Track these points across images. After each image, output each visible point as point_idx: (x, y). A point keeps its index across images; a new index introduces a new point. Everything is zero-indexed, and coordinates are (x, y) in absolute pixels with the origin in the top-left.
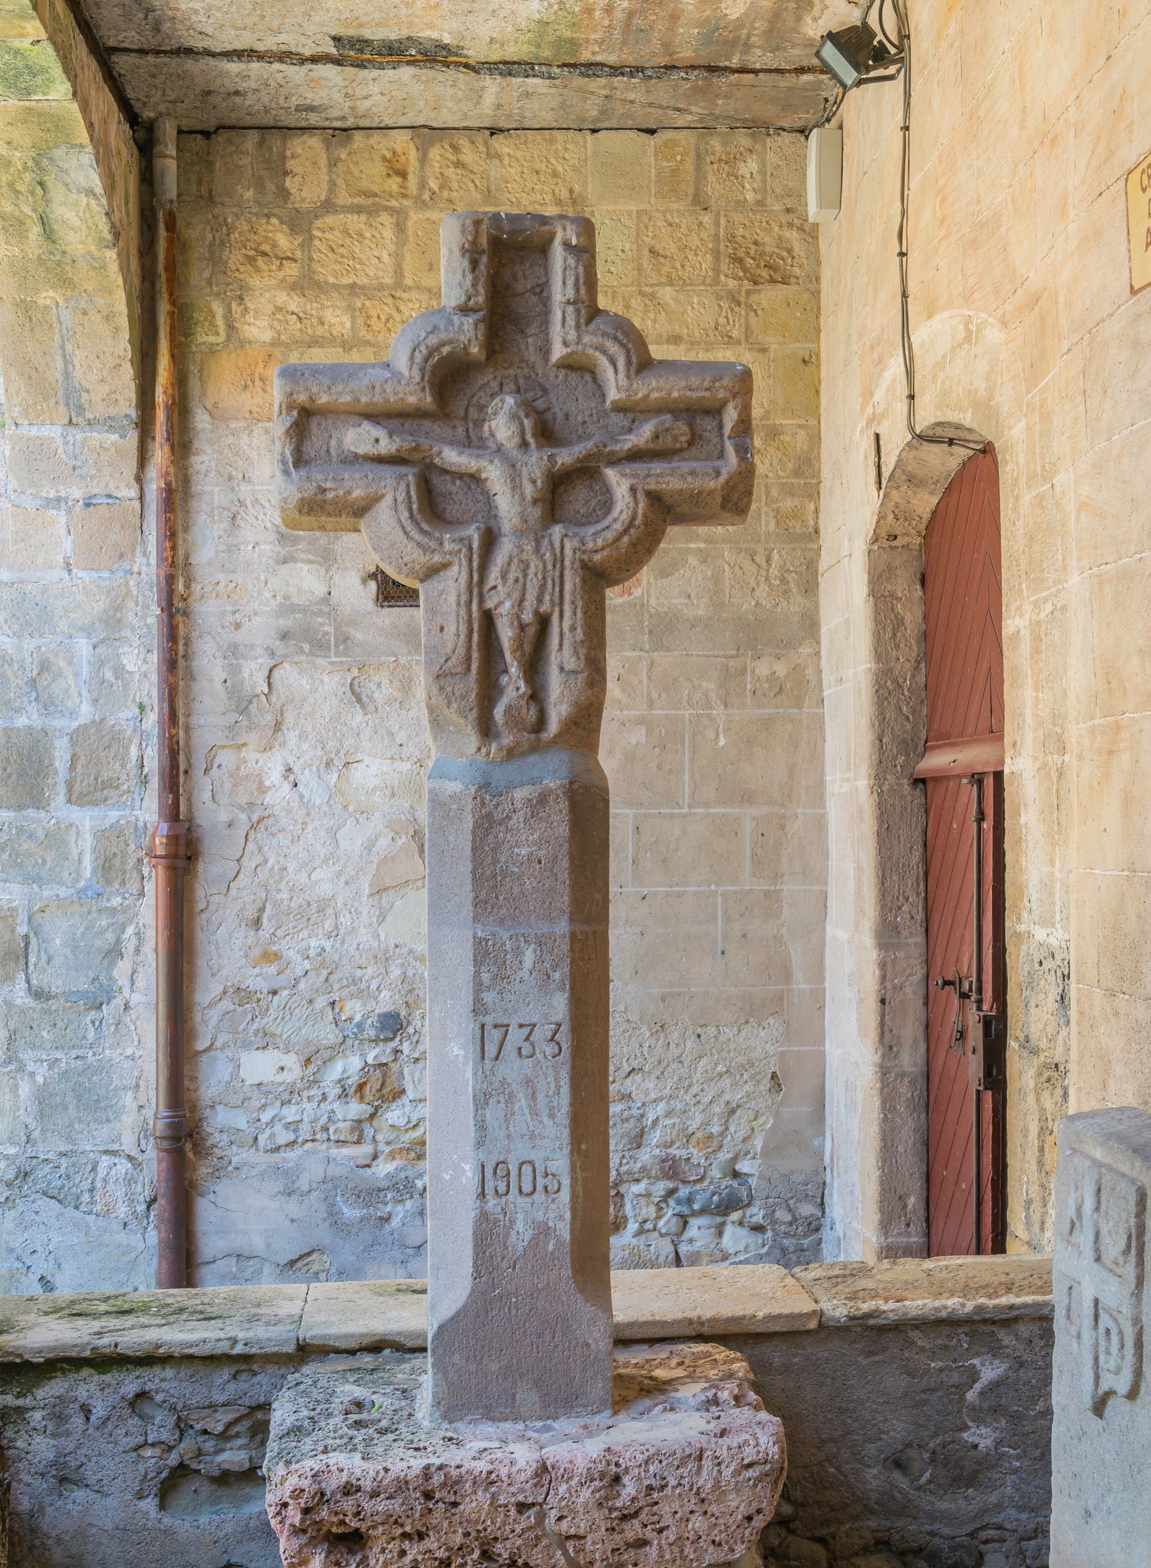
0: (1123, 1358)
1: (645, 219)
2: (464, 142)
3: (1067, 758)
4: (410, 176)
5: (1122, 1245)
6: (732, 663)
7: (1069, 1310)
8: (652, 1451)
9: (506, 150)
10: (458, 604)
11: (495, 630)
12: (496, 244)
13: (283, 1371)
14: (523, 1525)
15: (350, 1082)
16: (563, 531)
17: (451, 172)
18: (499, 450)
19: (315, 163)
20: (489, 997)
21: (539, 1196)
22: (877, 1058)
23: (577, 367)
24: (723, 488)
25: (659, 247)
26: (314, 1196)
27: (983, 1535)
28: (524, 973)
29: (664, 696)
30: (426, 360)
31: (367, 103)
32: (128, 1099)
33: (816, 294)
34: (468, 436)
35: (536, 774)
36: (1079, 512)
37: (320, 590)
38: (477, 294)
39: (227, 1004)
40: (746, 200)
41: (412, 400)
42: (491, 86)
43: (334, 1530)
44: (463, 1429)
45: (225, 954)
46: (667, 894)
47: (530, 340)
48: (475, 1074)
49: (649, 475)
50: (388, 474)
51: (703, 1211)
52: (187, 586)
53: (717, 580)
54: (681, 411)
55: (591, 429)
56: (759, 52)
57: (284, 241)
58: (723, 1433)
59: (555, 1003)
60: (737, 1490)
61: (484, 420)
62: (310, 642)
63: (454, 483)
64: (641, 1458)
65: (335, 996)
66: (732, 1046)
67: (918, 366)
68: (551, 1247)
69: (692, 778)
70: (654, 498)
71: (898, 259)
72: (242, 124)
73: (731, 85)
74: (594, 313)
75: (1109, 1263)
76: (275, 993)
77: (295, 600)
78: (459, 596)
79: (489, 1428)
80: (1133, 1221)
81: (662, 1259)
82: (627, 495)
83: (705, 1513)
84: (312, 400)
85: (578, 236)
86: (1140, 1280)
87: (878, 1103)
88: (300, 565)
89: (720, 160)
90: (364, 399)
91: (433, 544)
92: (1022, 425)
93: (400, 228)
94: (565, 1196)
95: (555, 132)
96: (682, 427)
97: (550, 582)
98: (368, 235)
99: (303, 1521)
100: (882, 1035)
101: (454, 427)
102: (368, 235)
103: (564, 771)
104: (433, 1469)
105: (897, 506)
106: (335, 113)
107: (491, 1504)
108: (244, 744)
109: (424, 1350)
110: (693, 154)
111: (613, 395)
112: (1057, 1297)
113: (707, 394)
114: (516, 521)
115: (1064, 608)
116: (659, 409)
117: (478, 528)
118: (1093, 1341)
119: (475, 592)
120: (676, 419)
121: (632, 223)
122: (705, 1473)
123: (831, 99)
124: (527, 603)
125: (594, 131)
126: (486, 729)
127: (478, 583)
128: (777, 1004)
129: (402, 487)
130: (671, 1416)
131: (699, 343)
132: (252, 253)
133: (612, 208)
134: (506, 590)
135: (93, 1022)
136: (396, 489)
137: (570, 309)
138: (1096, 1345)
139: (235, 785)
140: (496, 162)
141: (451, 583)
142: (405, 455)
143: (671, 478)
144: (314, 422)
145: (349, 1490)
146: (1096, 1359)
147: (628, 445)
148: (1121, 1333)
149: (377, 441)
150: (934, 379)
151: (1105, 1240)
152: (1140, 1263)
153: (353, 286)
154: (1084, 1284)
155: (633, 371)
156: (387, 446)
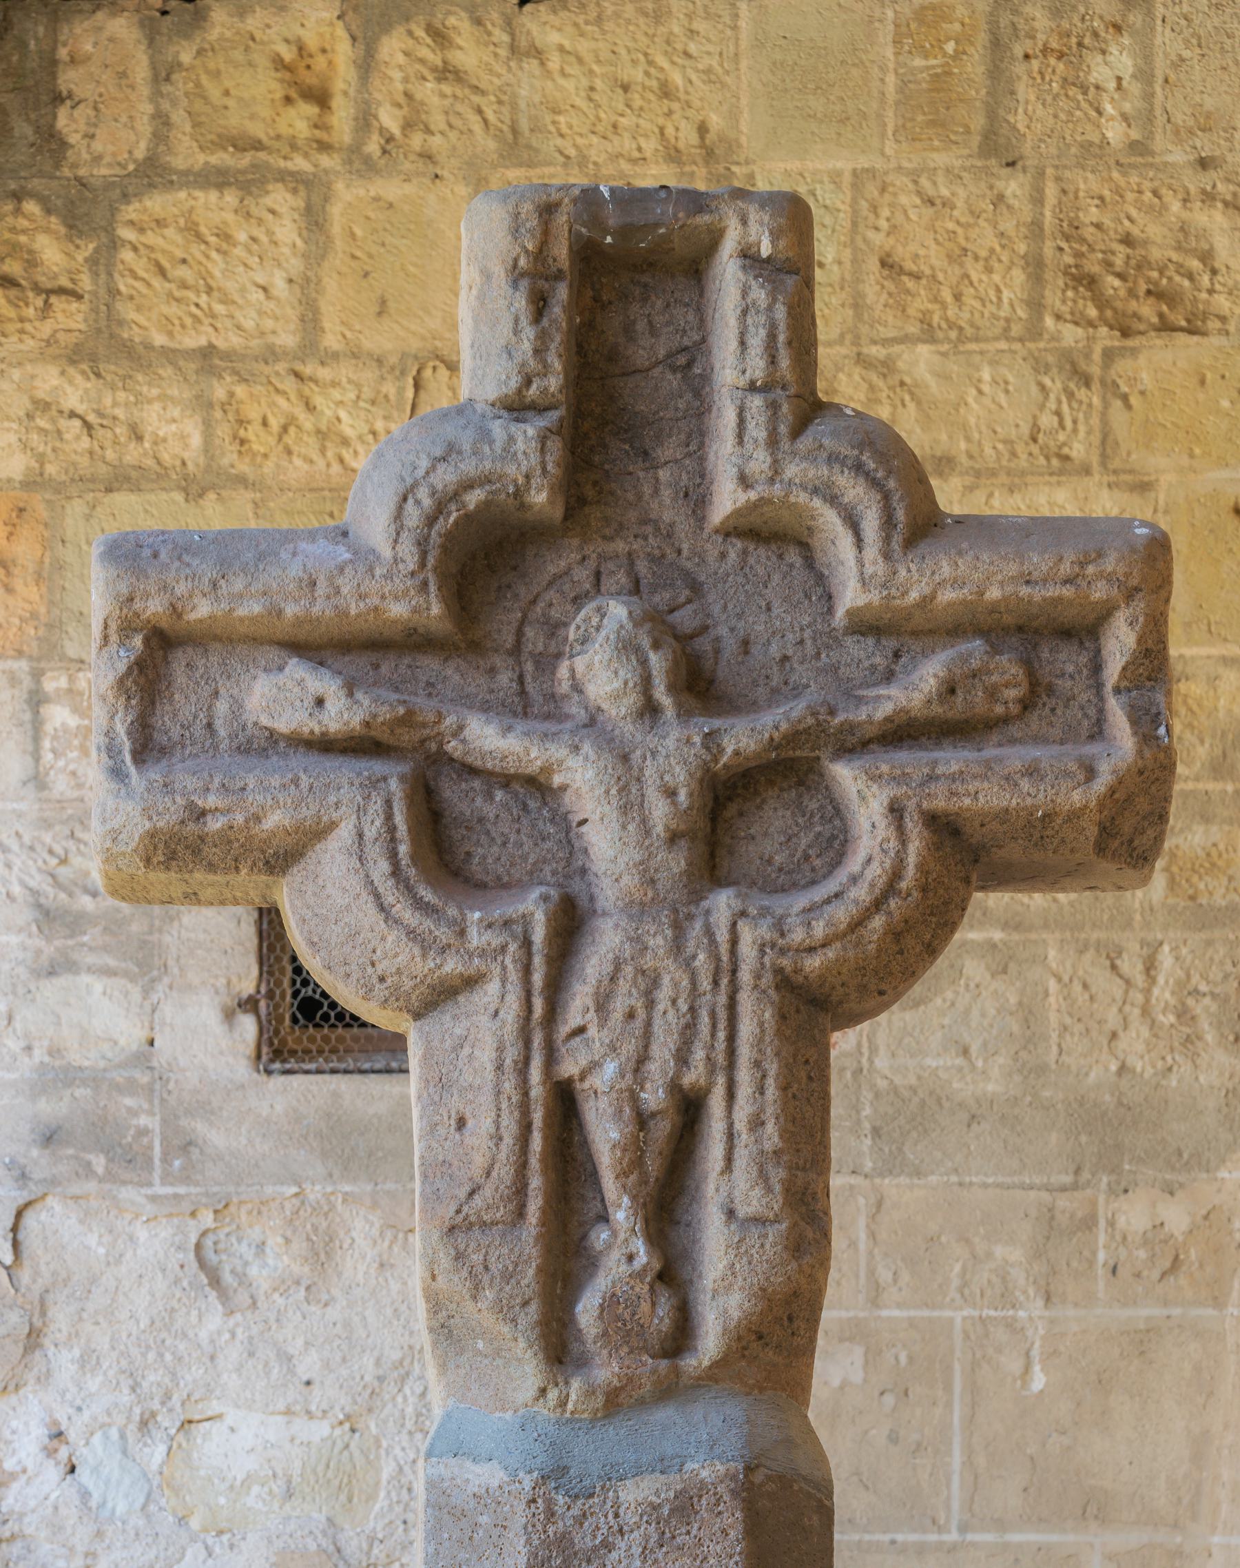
1: (872, 190)
4: (337, 102)
6: (1063, 1202)
9: (554, 38)
10: (499, 1068)
11: (581, 1126)
12: (591, 260)
16: (737, 905)
17: (428, 91)
18: (592, 722)
19: (123, 75)
24: (1101, 806)
25: (902, 254)
29: (905, 1277)
30: (431, 521)
34: (523, 692)
35: (668, 1448)
37: (130, 1034)
38: (546, 370)
40: (1104, 142)
41: (398, 610)
47: (664, 474)
49: (932, 778)
50: (345, 774)
53: (1029, 1013)
54: (1006, 630)
55: (801, 673)
57: (53, 253)
61: (559, 656)
62: (107, 1151)
63: (489, 796)
69: (969, 1463)
70: (944, 828)
74: (810, 409)
77: (75, 1057)
78: (500, 1049)
82: (882, 823)
85: (775, 236)
88: (85, 979)
89: (1046, 50)
90: (290, 610)
91: (444, 934)
93: (314, 220)
96: (1008, 668)
97: (705, 1019)
98: (242, 237)
101: (492, 671)
102: (242, 237)
103: (733, 1443)
110: (982, 38)
111: (851, 596)
113: (1067, 592)
114: (630, 881)
116: (955, 628)
117: (545, 898)
119: (538, 1039)
120: (995, 650)
124: (653, 1067)
126: (559, 1348)
129: (376, 805)
131: (993, 473)
136: (361, 811)
137: (756, 403)
140: (532, 65)
141: (484, 1020)
142: (384, 736)
143: (981, 783)
144: (179, 660)
147: (884, 711)
149: (320, 702)
153: (208, 352)
156: (342, 714)
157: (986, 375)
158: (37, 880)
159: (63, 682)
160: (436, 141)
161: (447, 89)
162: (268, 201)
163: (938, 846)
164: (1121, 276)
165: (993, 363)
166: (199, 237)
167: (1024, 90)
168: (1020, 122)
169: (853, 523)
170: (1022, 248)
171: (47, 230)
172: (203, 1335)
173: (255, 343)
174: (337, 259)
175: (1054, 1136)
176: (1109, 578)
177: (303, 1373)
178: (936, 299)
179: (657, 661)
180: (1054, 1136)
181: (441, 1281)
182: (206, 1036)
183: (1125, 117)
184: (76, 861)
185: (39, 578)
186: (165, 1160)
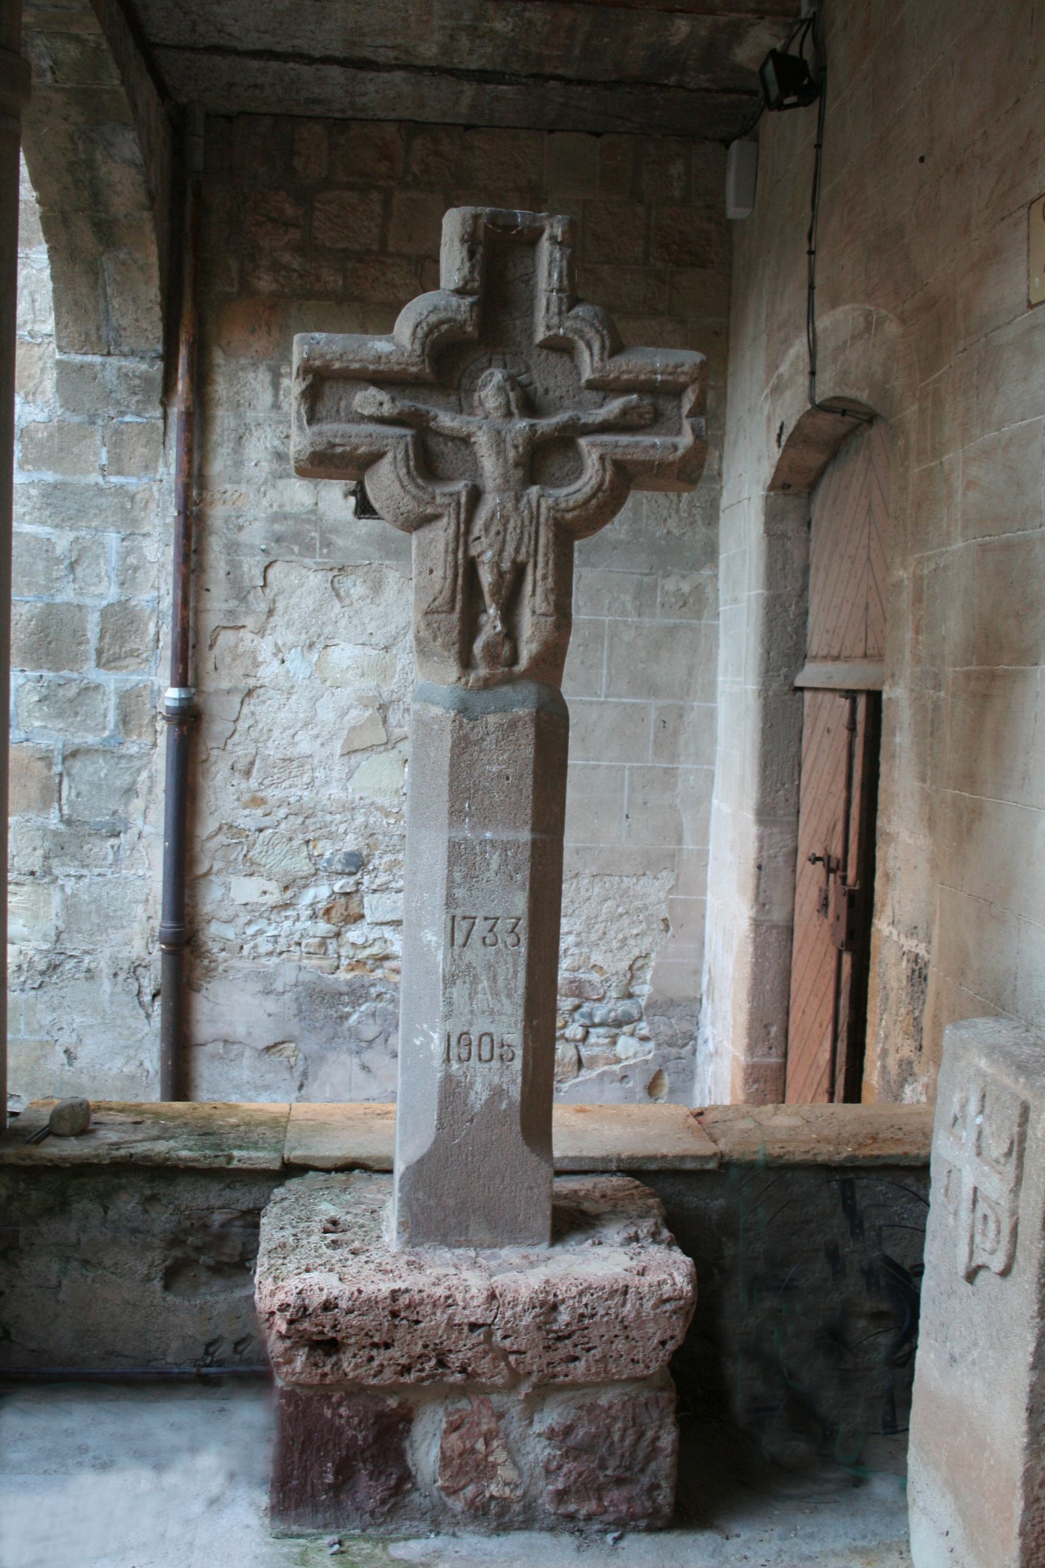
0: (998, 1242)
5: (1005, 1149)
6: (646, 579)
7: (947, 1190)
8: (585, 1285)
10: (446, 551)
14: (474, 1341)
15: (320, 906)
20: (459, 893)
21: (496, 1064)
22: (752, 913)
28: (491, 874)
31: (364, 100)
32: (139, 909)
38: (473, 280)
39: (222, 838)
42: (469, 90)
43: (315, 1338)
45: (223, 799)
46: (585, 767)
48: (445, 958)
51: (601, 1025)
52: (200, 494)
59: (516, 901)
62: (299, 544)
64: (574, 1291)
65: (310, 836)
66: (631, 893)
67: (820, 347)
68: (504, 1106)
71: (806, 257)
76: (261, 830)
77: (287, 509)
78: (447, 544)
79: (446, 1254)
80: (1016, 1129)
81: (566, 1060)
83: (627, 1337)
85: (563, 233)
86: (1019, 1180)
87: (751, 950)
92: (915, 407)
93: (387, 204)
94: (518, 1064)
97: (526, 536)
99: (288, 1330)
100: (757, 894)
107: (448, 1324)
108: (243, 627)
109: (390, 1172)
115: (946, 568)
118: (969, 1222)
122: (629, 1306)
124: (506, 554)
125: (551, 131)
126: (466, 662)
127: (463, 535)
128: (671, 860)
129: (402, 447)
130: (598, 1250)
135: (112, 847)
138: (973, 1226)
139: (234, 660)
141: (441, 533)
145: (328, 1306)
146: (972, 1237)
149: (381, 404)
151: (989, 1141)
152: (1020, 1165)
153: (345, 250)
154: (964, 1173)
155: (606, 353)
156: (387, 410)
169: (590, 347)
181: (422, 634)
186: (321, 549)
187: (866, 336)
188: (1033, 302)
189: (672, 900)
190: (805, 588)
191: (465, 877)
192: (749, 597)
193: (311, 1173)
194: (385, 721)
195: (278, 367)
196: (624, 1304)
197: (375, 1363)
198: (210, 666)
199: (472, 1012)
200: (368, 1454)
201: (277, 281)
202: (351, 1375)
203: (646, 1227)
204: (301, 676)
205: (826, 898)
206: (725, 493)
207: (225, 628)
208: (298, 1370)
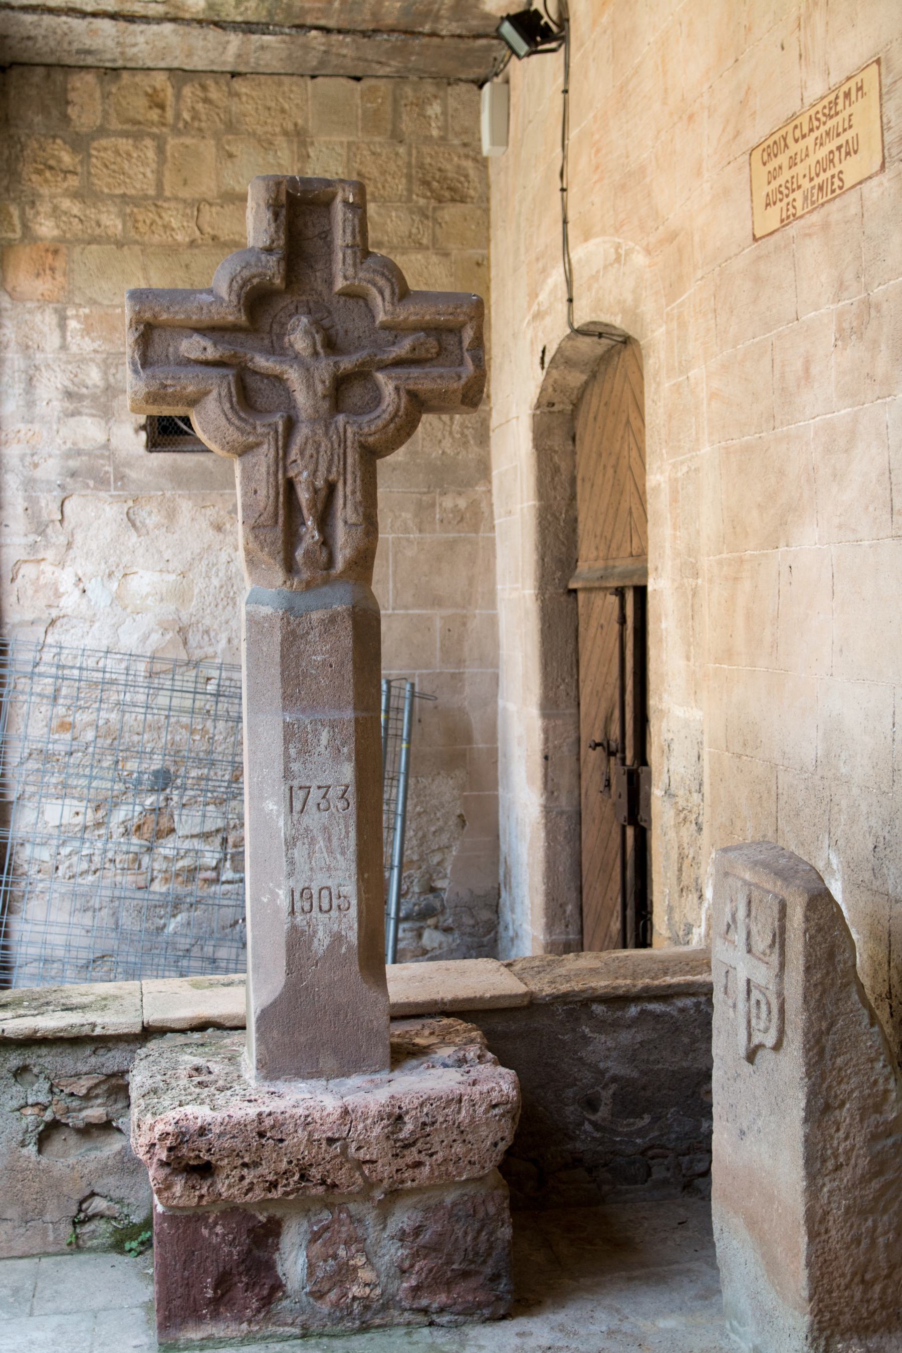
0: (770, 1021)
1: (354, 149)
2: (210, 83)
3: (700, 581)
4: (168, 109)
5: (769, 940)
6: (424, 498)
7: (726, 988)
8: (425, 1097)
10: (268, 473)
13: (132, 1047)
17: (200, 106)
18: (296, 357)
20: (295, 766)
21: (334, 913)
23: (353, 295)
26: (105, 912)
27: (650, 1153)
28: (322, 749)
30: (242, 288)
31: (135, 50)
33: (487, 211)
36: (710, 399)
37: (101, 438)
38: (278, 240)
39: (32, 765)
41: (231, 318)
42: (235, 40)
43: (191, 1163)
44: (280, 1086)
47: (318, 274)
48: (286, 824)
49: (408, 378)
50: (215, 373)
56: (445, 22)
57: (67, 158)
58: (474, 1083)
59: (345, 771)
60: (487, 1124)
61: (284, 334)
62: (94, 479)
64: (416, 1102)
66: (428, 792)
67: (576, 276)
68: (343, 950)
69: (395, 586)
70: (413, 395)
71: (559, 194)
72: (33, 61)
73: (422, 46)
74: (366, 254)
75: (757, 954)
77: (82, 446)
78: (268, 467)
80: (776, 923)
84: (155, 316)
86: (782, 966)
88: (84, 418)
90: (194, 317)
91: (249, 428)
93: (160, 150)
94: (353, 912)
95: (282, 77)
96: (432, 343)
97: (336, 457)
98: (135, 155)
99: (168, 1157)
100: (546, 783)
101: (262, 339)
104: (264, 1115)
105: (555, 382)
106: (108, 56)
108: (43, 560)
109: (243, 1028)
111: (381, 317)
112: (716, 978)
113: (451, 317)
115: (697, 470)
116: (415, 329)
119: (281, 464)
120: (428, 336)
121: (344, 152)
122: (463, 1112)
123: (500, 59)
125: (313, 77)
126: (290, 567)
129: (225, 385)
131: (396, 248)
132: (42, 167)
133: (327, 139)
134: (304, 463)
137: (349, 251)
139: (36, 591)
140: (236, 99)
141: (263, 457)
142: (226, 360)
143: (425, 380)
144: (156, 334)
145: (203, 1131)
146: (749, 1022)
147: (394, 355)
148: (768, 1004)
149: (205, 349)
150: (589, 288)
151: (755, 938)
152: (782, 953)
153: (124, 196)
154: (739, 969)
156: (211, 353)
157: (394, 214)
158: (68, 383)
159: (74, 312)
160: (203, 125)
161: (207, 106)
162: (144, 143)
163: (411, 401)
164: (438, 182)
165: (396, 210)
166: (120, 155)
167: (405, 117)
168: (404, 128)
170: (405, 171)
171: (65, 150)
172: (130, 545)
173: (141, 193)
174: (169, 165)
175: (421, 475)
176: (465, 314)
177: (166, 557)
178: (376, 187)
179: (318, 338)
180: (421, 475)
181: (250, 545)
182: (130, 439)
183: (439, 128)
184: (80, 376)
185: (64, 274)
186: (115, 482)
187: (616, 265)
188: (758, 236)
189: (466, 797)
190: (573, 497)
191: (299, 753)
192: (522, 509)
193: (169, 1035)
194: (185, 643)
195: (65, 309)
196: (459, 1112)
197: (247, 1181)
198: (13, 599)
199: (311, 869)
200: (242, 1268)
201: (58, 227)
202: (225, 1195)
203: (472, 1052)
204: (102, 605)
205: (608, 780)
206: (494, 413)
207: (25, 561)
208: (178, 1194)
